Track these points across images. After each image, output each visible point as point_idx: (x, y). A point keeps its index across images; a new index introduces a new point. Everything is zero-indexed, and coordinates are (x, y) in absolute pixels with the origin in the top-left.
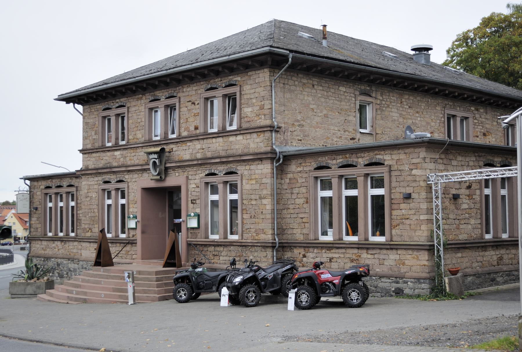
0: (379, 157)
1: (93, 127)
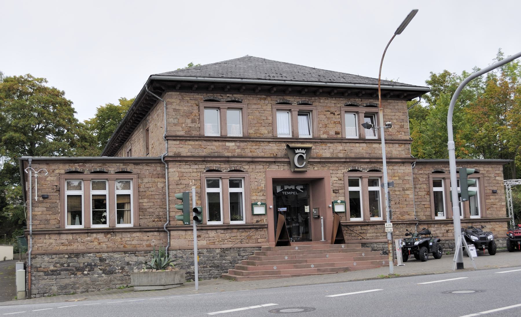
0: (129, 168)
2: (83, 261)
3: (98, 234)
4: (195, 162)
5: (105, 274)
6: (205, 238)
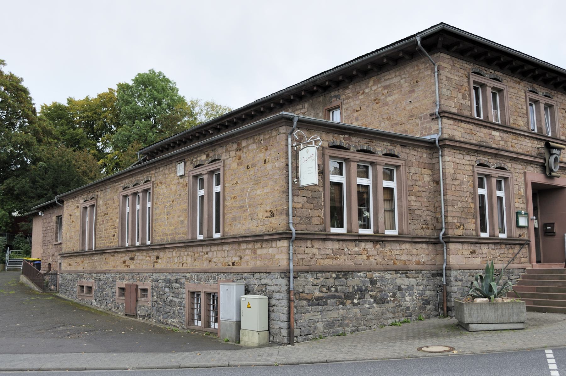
1: (460, 87)
2: (354, 282)
3: (367, 244)
4: (469, 151)
5: (377, 304)
6: (479, 254)
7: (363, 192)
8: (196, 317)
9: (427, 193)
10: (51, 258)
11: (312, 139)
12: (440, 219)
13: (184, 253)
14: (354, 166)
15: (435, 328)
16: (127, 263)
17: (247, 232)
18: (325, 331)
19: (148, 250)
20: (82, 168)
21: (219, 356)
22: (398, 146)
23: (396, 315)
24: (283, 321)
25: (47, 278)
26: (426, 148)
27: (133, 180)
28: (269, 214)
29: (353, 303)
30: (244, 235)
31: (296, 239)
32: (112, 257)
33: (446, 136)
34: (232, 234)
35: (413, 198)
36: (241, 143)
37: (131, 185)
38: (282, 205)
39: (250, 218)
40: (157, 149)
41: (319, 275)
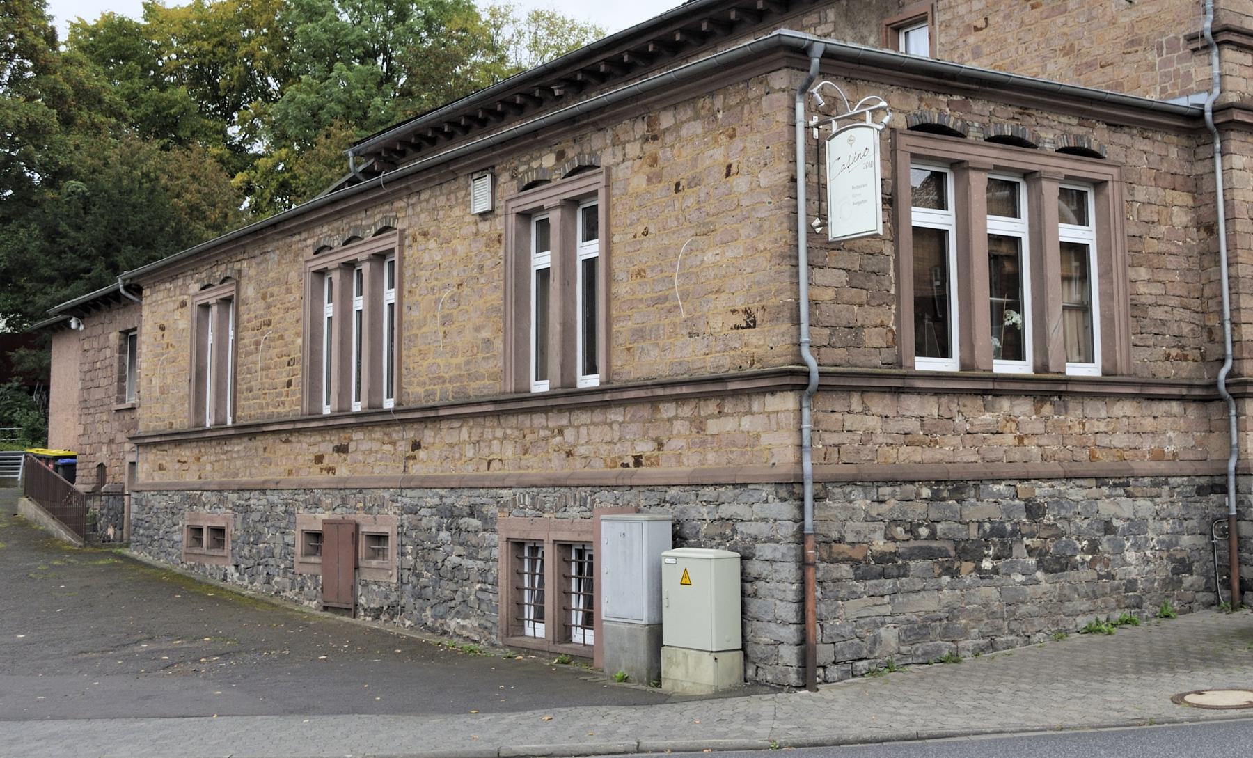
3: (1016, 402)
5: (1046, 571)
7: (1004, 253)
8: (529, 612)
9: (1182, 260)
10: (104, 449)
11: (863, 105)
12: (1217, 332)
13: (492, 430)
14: (978, 182)
15: (1210, 638)
16: (326, 462)
17: (677, 369)
18: (904, 649)
19: (389, 424)
20: (188, 196)
21: (606, 722)
22: (1100, 125)
23: (1099, 602)
24: (785, 623)
25: (95, 506)
26: (1178, 131)
27: (345, 226)
28: (740, 319)
29: (978, 569)
30: (670, 379)
31: (822, 389)
32: (284, 446)
33: (1233, 98)
34: (632, 376)
35: (1143, 273)
36: (657, 119)
37: (336, 242)
38: (779, 292)
39: (685, 332)
40: (404, 141)
41: (886, 490)
